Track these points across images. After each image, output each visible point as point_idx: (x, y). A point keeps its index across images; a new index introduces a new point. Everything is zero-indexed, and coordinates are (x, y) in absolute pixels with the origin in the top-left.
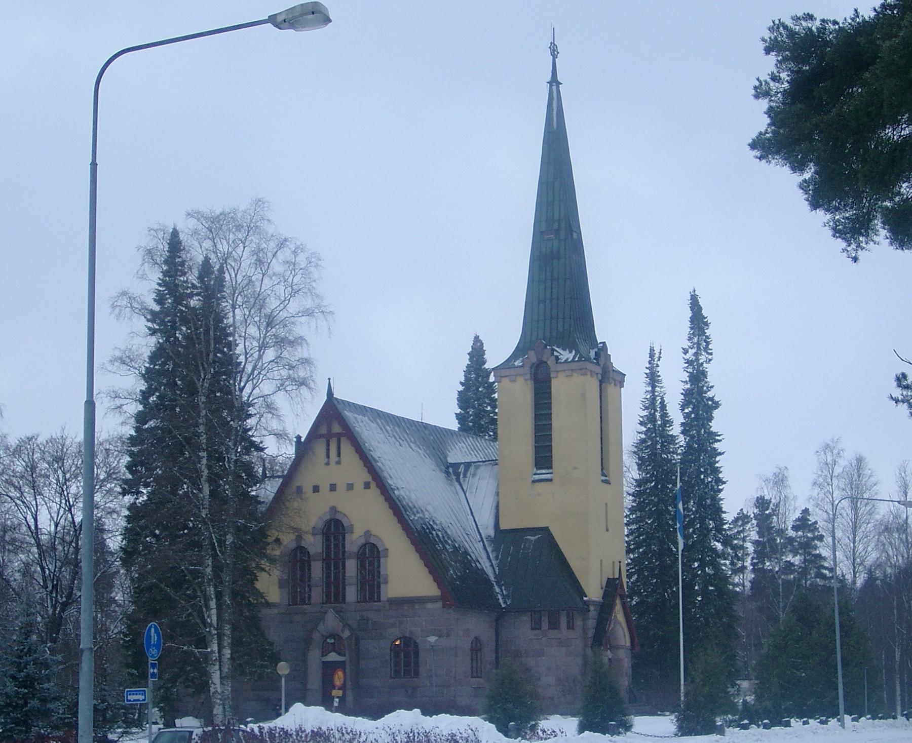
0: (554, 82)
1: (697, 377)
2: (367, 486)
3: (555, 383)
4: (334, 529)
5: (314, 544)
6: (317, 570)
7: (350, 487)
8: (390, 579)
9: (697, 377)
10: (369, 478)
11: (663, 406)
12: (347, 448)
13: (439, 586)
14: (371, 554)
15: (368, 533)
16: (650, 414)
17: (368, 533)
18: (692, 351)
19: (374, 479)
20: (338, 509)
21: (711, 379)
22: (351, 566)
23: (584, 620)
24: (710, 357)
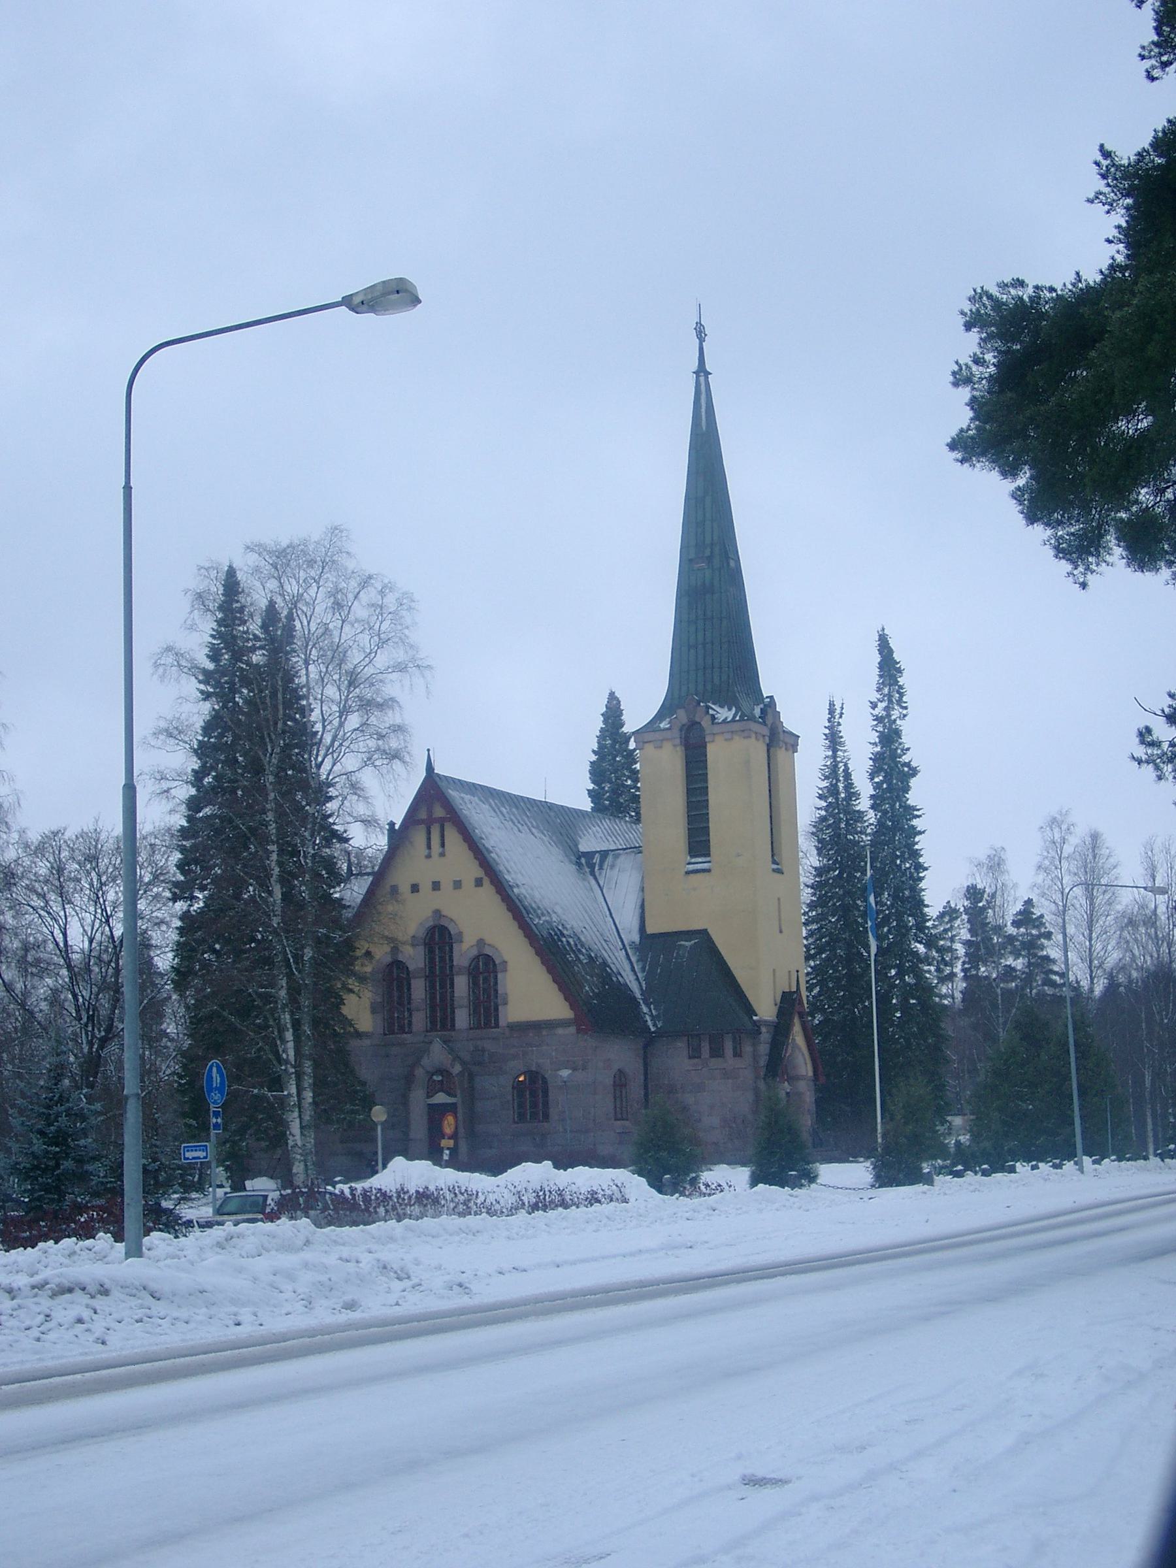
0: (702, 371)
1: (889, 738)
2: (479, 883)
3: (711, 750)
4: (439, 938)
5: (414, 958)
6: (419, 990)
7: (458, 885)
8: (511, 999)
9: (889, 738)
10: (480, 873)
11: (847, 775)
12: (453, 837)
13: (572, 1007)
14: (486, 968)
15: (481, 942)
16: (831, 784)
17: (481, 942)
18: (881, 705)
19: (487, 874)
20: (443, 913)
21: (906, 740)
22: (461, 984)
23: (754, 1045)
24: (905, 712)
